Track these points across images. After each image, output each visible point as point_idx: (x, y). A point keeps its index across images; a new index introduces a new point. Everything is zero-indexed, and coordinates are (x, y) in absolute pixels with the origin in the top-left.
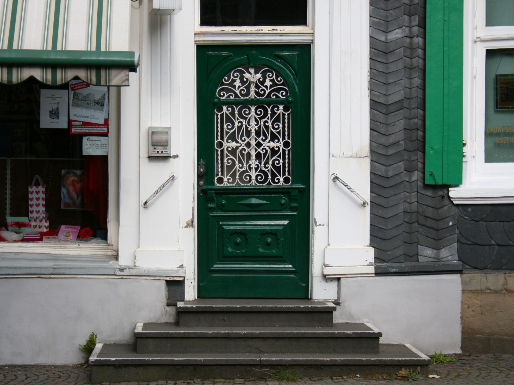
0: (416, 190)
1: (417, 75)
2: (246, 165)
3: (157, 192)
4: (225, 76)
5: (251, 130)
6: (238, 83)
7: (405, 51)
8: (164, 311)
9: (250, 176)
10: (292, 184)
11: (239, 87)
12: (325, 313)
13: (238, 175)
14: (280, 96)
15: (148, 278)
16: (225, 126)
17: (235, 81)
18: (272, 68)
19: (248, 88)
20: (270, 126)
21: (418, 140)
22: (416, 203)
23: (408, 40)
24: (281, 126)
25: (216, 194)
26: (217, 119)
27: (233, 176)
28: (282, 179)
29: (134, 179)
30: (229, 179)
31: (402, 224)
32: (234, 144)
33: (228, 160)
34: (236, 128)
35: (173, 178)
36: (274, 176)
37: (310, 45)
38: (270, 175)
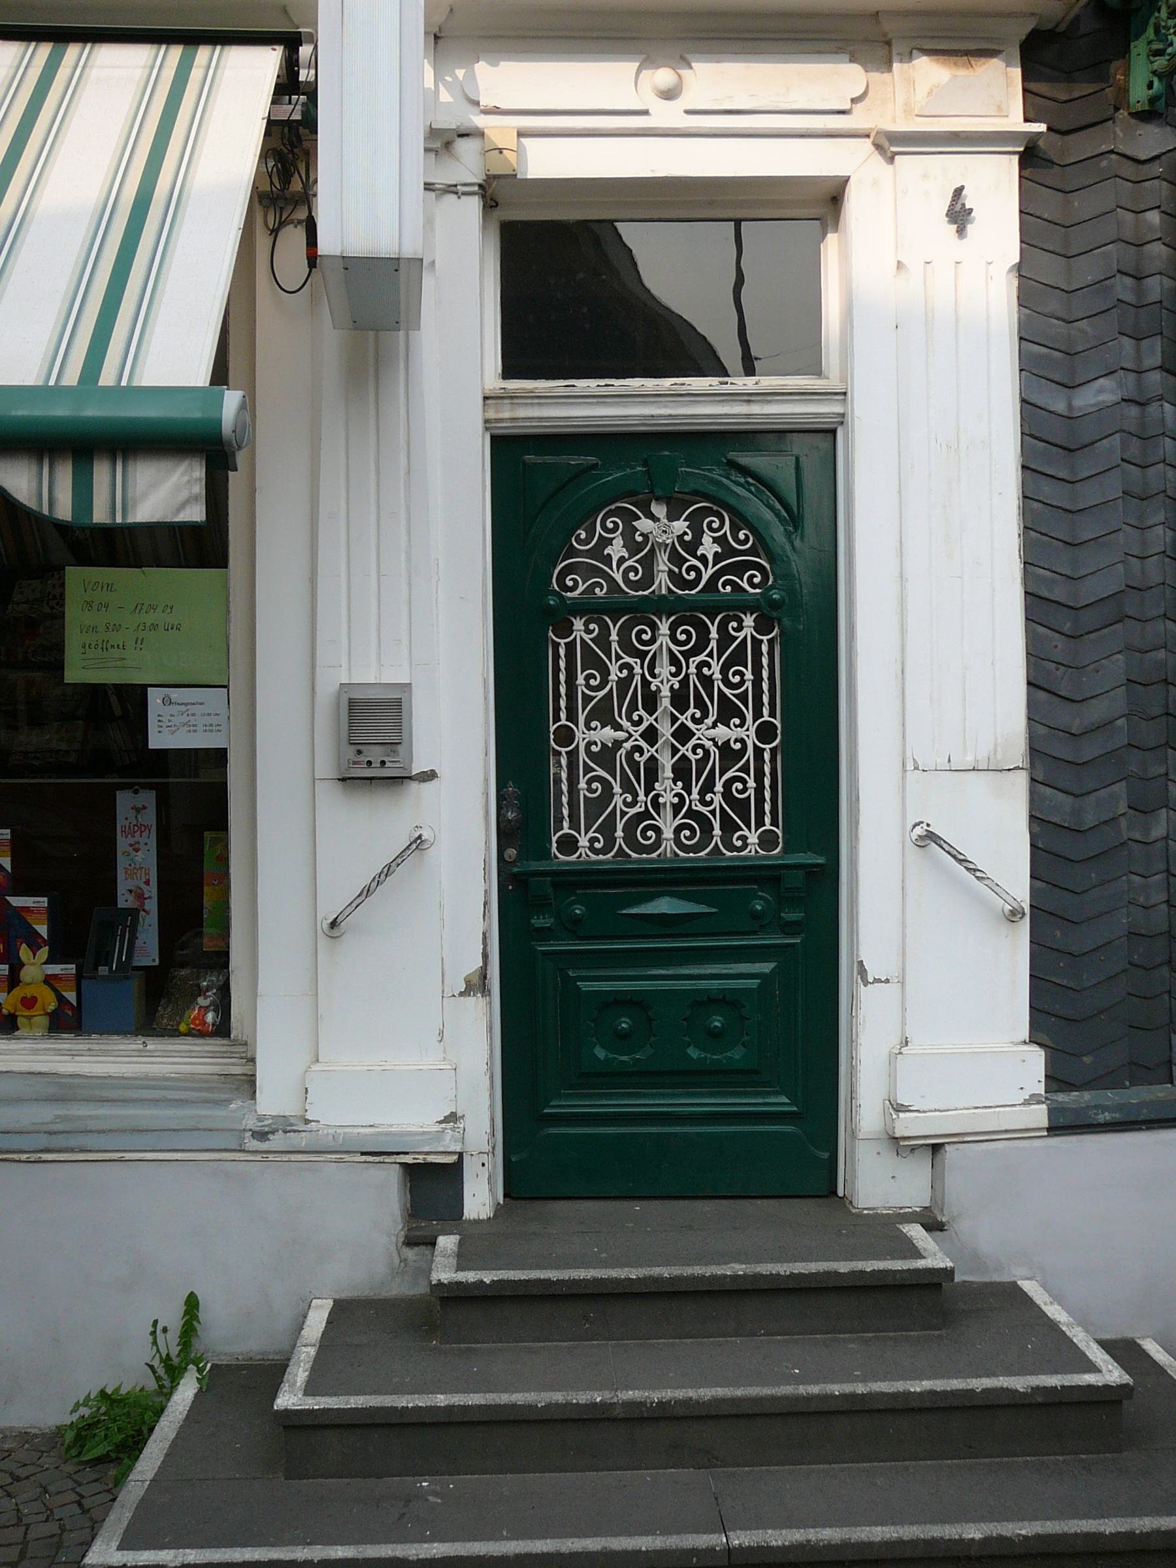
0: (1163, 866)
1: (1161, 517)
2: (646, 795)
3: (367, 892)
4: (578, 528)
5: (659, 690)
6: (617, 550)
7: (1124, 445)
8: (397, 1261)
9: (658, 830)
10: (785, 850)
11: (622, 560)
12: (885, 1230)
13: (620, 827)
14: (746, 586)
15: (346, 1157)
16: (581, 680)
17: (609, 542)
18: (722, 504)
19: (648, 562)
20: (717, 676)
21: (1167, 714)
22: (1164, 907)
23: (1134, 411)
24: (749, 676)
25: (555, 885)
26: (557, 657)
27: (608, 829)
28: (753, 839)
29: (294, 848)
30: (593, 840)
31: (1124, 971)
32: (607, 734)
33: (589, 783)
34: (612, 684)
35: (418, 843)
36: (729, 827)
37: (834, 432)
38: (717, 825)
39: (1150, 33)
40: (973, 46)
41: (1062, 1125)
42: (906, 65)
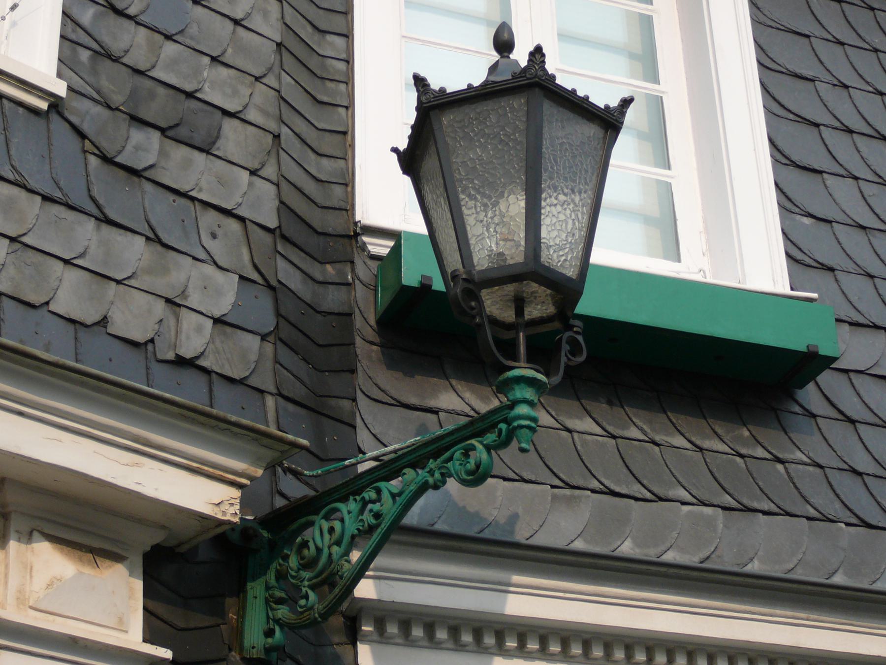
39: (271, 577)
40: (96, 544)
42: (23, 546)
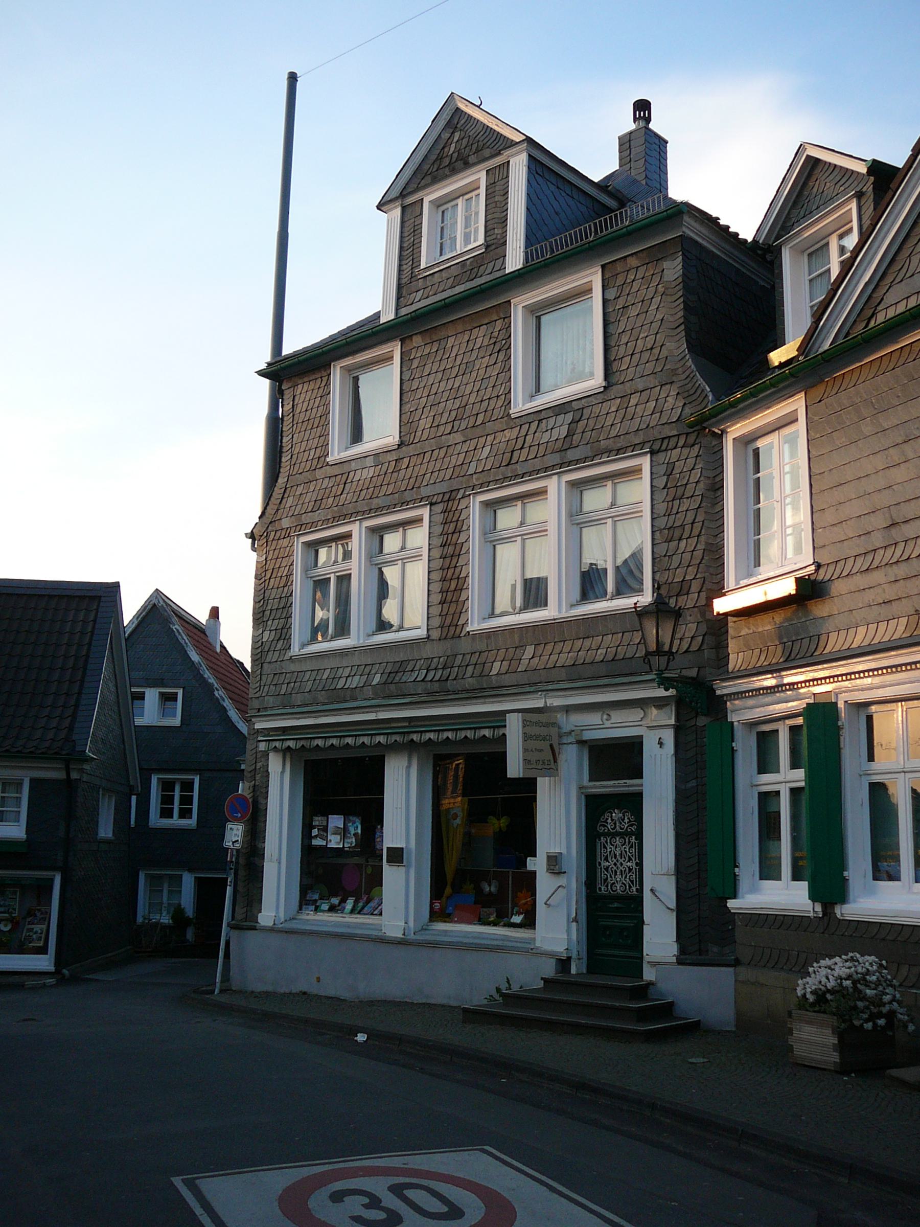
6: (609, 821)
19: (615, 824)
36: (630, 887)
41: (680, 962)
